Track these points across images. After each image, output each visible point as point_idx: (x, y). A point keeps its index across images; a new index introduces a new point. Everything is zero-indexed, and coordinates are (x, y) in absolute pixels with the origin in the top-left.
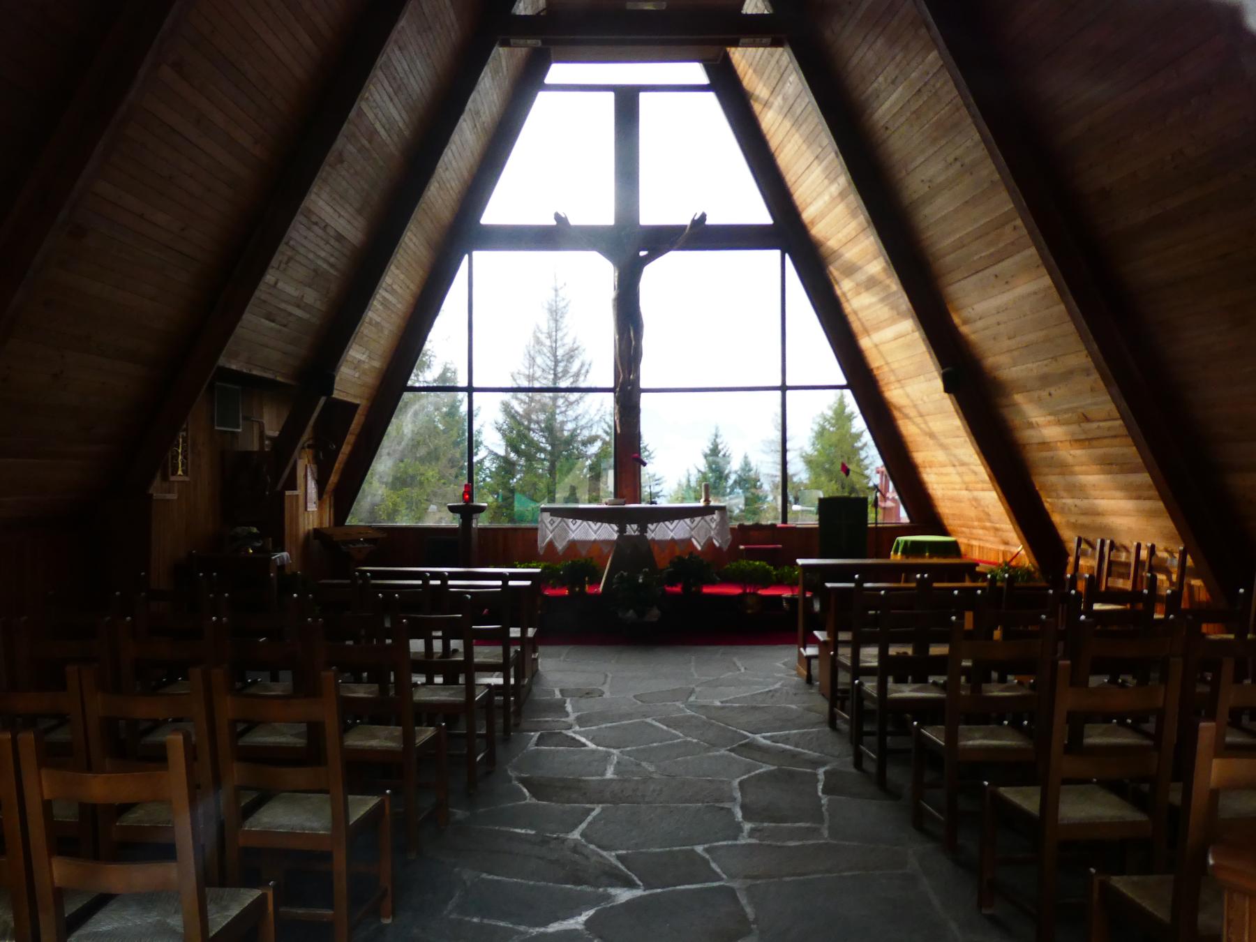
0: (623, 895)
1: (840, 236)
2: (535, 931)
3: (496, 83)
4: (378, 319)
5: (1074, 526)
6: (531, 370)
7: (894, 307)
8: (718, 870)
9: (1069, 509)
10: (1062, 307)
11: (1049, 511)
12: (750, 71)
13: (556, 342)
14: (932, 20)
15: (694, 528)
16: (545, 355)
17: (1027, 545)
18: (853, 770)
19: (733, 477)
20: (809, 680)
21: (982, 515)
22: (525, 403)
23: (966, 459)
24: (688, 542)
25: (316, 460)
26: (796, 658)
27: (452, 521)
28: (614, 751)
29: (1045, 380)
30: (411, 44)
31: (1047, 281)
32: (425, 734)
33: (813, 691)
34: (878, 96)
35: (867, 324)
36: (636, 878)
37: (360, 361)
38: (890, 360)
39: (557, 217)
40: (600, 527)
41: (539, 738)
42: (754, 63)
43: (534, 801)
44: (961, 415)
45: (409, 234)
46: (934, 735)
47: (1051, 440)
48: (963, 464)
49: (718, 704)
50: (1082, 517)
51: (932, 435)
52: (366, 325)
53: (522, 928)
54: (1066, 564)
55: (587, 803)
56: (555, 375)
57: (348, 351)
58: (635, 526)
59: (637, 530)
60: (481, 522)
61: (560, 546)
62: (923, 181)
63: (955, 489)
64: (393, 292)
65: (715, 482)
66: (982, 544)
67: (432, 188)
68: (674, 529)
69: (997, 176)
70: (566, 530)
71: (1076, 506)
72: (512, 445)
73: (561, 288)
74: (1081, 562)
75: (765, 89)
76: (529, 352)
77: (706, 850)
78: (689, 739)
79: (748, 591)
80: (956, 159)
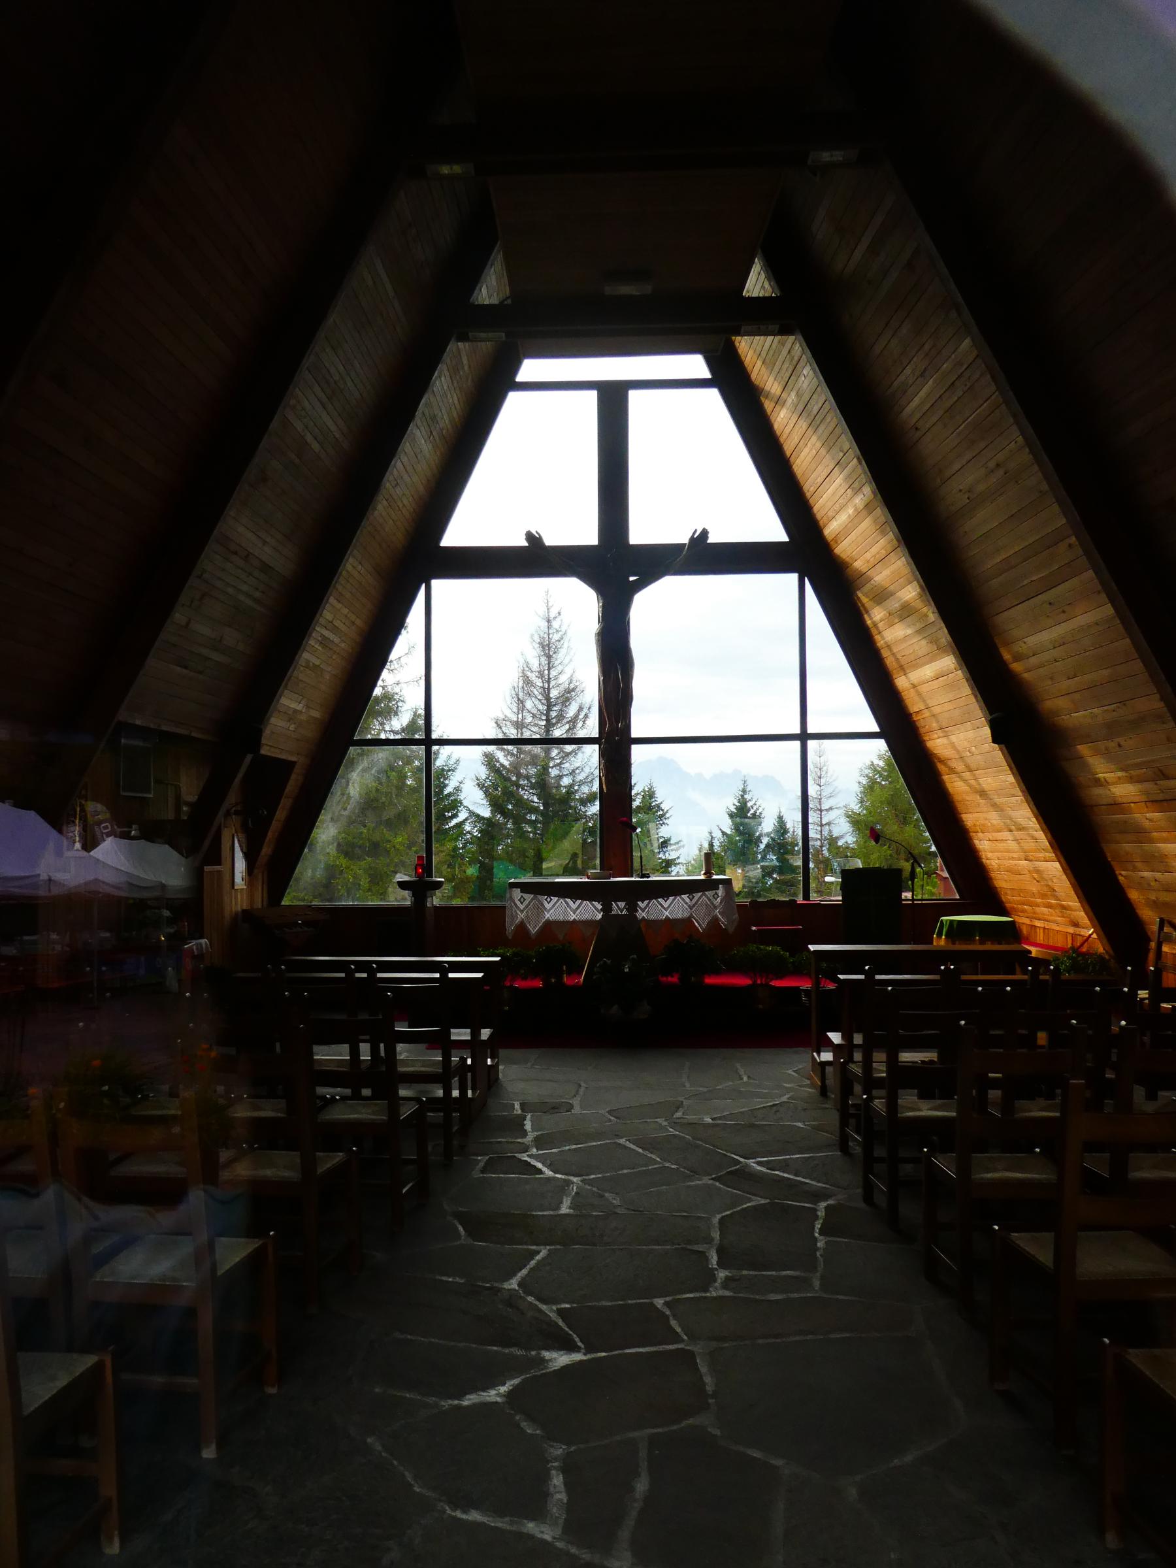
0: (560, 1359)
1: (868, 555)
2: (447, 1404)
3: (455, 384)
4: (317, 662)
5: (1155, 905)
6: (520, 716)
7: (933, 641)
8: (679, 1330)
9: (1149, 885)
10: (1128, 640)
11: (1125, 886)
12: (759, 363)
13: (549, 682)
14: (963, 302)
15: (694, 906)
16: (536, 697)
17: (1099, 928)
18: (862, 1205)
19: (765, 840)
20: (824, 1091)
21: (1045, 890)
22: (512, 754)
23: (1023, 822)
24: (687, 922)
25: (245, 828)
26: (809, 1066)
27: (404, 899)
28: (575, 1179)
29: (1112, 729)
30: (347, 342)
31: (1109, 610)
32: (330, 1161)
33: (827, 1106)
34: (905, 392)
35: (903, 661)
36: (577, 1339)
37: (295, 711)
38: (931, 703)
39: (530, 536)
40: (580, 905)
41: (487, 1163)
42: (764, 354)
43: (470, 1241)
44: (1015, 770)
45: (351, 560)
46: (945, 1165)
47: (1124, 800)
48: (1021, 829)
49: (708, 1120)
50: (1165, 894)
51: (983, 793)
52: (302, 668)
53: (432, 1400)
54: (1148, 950)
55: (533, 1245)
56: (548, 720)
57: (279, 700)
58: (622, 904)
59: (625, 907)
60: (436, 900)
61: (533, 930)
62: (960, 491)
63: (1013, 859)
64: (335, 629)
65: (743, 846)
66: (1047, 925)
67: (380, 507)
68: (669, 907)
69: (1045, 487)
70: (540, 909)
71: (1156, 880)
72: (496, 805)
73: (555, 618)
74: (1165, 949)
75: (776, 384)
76: (517, 695)
77: (666, 1304)
78: (667, 1165)
79: (759, 982)
80: (998, 465)
